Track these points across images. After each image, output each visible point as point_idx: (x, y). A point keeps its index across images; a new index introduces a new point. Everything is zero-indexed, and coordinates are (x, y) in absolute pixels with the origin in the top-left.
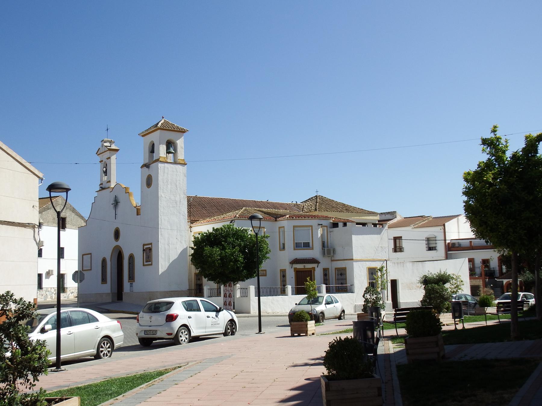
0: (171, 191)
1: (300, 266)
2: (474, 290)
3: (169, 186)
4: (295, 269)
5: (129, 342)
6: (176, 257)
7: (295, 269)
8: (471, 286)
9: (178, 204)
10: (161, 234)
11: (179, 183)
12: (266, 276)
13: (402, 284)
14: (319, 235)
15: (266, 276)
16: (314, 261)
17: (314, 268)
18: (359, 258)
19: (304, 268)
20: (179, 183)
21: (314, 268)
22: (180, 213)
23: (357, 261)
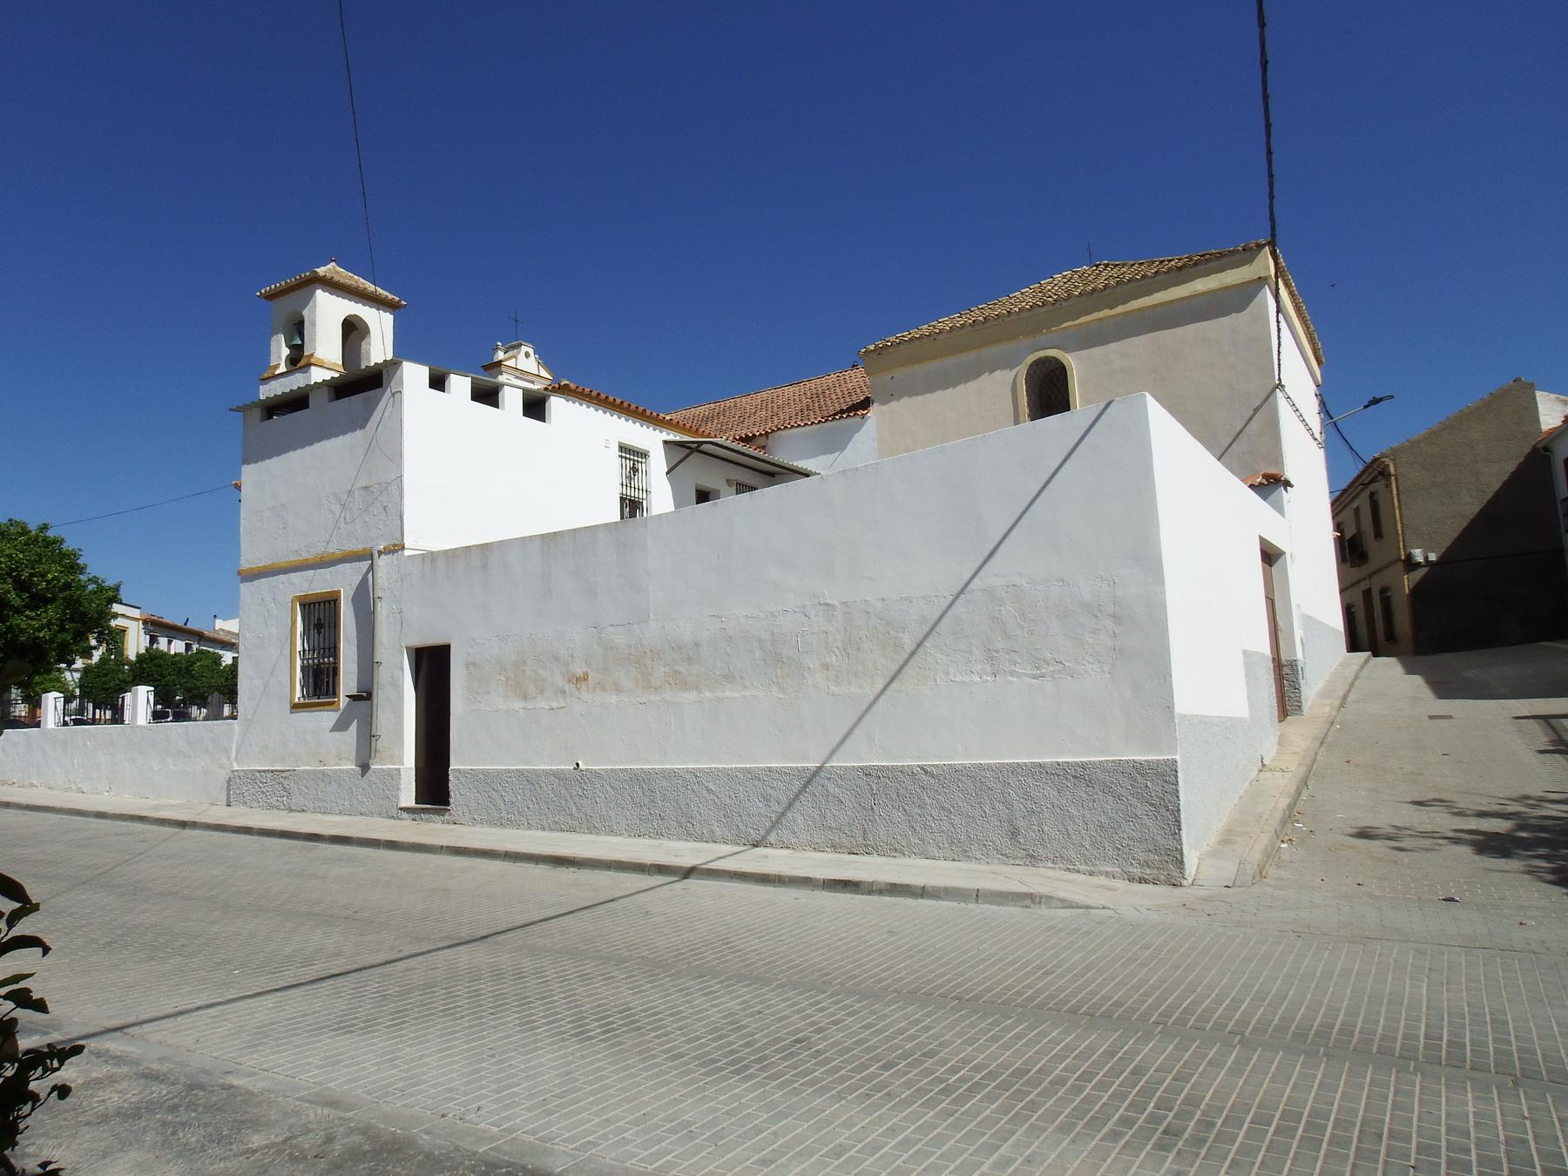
13: (470, 665)
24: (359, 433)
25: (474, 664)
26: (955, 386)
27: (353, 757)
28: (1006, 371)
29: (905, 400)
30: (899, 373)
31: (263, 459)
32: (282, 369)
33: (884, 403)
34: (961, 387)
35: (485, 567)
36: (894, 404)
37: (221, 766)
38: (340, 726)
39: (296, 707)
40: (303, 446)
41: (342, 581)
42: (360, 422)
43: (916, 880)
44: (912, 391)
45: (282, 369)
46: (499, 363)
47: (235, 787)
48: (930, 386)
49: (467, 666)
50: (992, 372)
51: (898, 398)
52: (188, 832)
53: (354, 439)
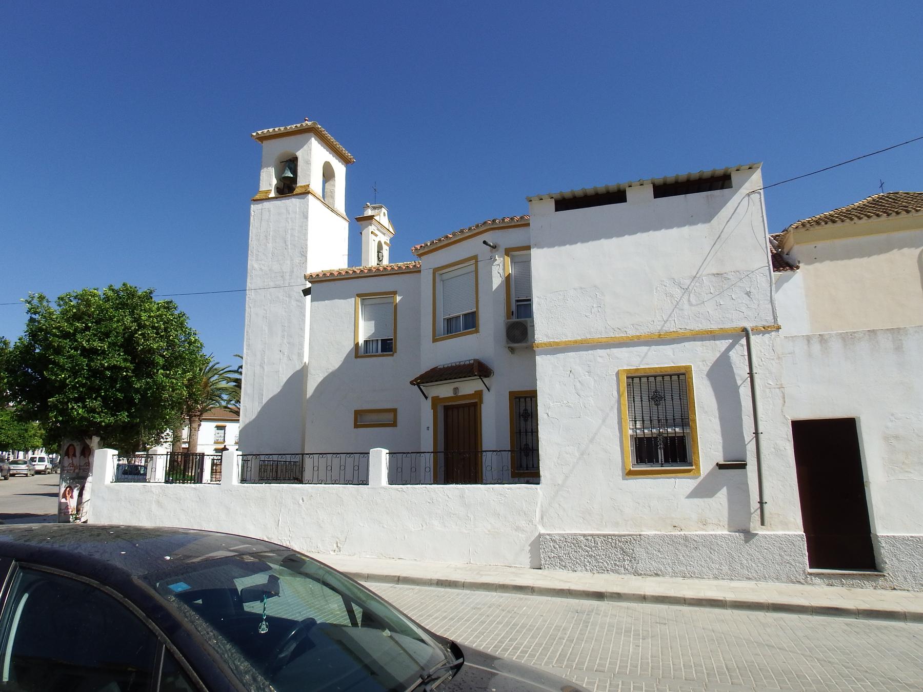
0: (273, 254)
1: (444, 390)
2: (492, 259)
3: (270, 245)
4: (436, 401)
5: (616, 524)
6: (277, 390)
7: (436, 401)
8: (436, 482)
9: (287, 277)
10: (249, 345)
11: (292, 235)
12: (394, 424)
13: (890, 439)
14: (497, 281)
15: (394, 424)
16: (480, 370)
17: (479, 394)
18: (569, 334)
19: (456, 397)
20: (292, 235)
21: (479, 394)
22: (290, 297)
23: (556, 348)
24: (701, 229)
25: (897, 437)
26: (869, 255)
27: (725, 519)
28: (913, 249)
29: (827, 263)
30: (820, 244)
31: (563, 243)
32: (272, 195)
33: (809, 262)
34: (875, 258)
35: (899, 348)
36: (817, 265)
37: (518, 529)
38: (704, 491)
39: (630, 474)
40: (620, 234)
41: (696, 359)
42: (708, 217)
43: (672, 593)
44: (834, 257)
45: (272, 195)
46: (371, 218)
47: (542, 552)
48: (849, 254)
49: (886, 438)
50: (900, 248)
51: (822, 261)
52: (603, 605)
53: (700, 230)
